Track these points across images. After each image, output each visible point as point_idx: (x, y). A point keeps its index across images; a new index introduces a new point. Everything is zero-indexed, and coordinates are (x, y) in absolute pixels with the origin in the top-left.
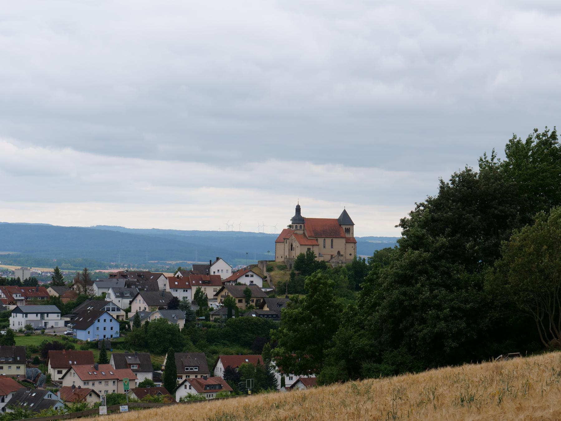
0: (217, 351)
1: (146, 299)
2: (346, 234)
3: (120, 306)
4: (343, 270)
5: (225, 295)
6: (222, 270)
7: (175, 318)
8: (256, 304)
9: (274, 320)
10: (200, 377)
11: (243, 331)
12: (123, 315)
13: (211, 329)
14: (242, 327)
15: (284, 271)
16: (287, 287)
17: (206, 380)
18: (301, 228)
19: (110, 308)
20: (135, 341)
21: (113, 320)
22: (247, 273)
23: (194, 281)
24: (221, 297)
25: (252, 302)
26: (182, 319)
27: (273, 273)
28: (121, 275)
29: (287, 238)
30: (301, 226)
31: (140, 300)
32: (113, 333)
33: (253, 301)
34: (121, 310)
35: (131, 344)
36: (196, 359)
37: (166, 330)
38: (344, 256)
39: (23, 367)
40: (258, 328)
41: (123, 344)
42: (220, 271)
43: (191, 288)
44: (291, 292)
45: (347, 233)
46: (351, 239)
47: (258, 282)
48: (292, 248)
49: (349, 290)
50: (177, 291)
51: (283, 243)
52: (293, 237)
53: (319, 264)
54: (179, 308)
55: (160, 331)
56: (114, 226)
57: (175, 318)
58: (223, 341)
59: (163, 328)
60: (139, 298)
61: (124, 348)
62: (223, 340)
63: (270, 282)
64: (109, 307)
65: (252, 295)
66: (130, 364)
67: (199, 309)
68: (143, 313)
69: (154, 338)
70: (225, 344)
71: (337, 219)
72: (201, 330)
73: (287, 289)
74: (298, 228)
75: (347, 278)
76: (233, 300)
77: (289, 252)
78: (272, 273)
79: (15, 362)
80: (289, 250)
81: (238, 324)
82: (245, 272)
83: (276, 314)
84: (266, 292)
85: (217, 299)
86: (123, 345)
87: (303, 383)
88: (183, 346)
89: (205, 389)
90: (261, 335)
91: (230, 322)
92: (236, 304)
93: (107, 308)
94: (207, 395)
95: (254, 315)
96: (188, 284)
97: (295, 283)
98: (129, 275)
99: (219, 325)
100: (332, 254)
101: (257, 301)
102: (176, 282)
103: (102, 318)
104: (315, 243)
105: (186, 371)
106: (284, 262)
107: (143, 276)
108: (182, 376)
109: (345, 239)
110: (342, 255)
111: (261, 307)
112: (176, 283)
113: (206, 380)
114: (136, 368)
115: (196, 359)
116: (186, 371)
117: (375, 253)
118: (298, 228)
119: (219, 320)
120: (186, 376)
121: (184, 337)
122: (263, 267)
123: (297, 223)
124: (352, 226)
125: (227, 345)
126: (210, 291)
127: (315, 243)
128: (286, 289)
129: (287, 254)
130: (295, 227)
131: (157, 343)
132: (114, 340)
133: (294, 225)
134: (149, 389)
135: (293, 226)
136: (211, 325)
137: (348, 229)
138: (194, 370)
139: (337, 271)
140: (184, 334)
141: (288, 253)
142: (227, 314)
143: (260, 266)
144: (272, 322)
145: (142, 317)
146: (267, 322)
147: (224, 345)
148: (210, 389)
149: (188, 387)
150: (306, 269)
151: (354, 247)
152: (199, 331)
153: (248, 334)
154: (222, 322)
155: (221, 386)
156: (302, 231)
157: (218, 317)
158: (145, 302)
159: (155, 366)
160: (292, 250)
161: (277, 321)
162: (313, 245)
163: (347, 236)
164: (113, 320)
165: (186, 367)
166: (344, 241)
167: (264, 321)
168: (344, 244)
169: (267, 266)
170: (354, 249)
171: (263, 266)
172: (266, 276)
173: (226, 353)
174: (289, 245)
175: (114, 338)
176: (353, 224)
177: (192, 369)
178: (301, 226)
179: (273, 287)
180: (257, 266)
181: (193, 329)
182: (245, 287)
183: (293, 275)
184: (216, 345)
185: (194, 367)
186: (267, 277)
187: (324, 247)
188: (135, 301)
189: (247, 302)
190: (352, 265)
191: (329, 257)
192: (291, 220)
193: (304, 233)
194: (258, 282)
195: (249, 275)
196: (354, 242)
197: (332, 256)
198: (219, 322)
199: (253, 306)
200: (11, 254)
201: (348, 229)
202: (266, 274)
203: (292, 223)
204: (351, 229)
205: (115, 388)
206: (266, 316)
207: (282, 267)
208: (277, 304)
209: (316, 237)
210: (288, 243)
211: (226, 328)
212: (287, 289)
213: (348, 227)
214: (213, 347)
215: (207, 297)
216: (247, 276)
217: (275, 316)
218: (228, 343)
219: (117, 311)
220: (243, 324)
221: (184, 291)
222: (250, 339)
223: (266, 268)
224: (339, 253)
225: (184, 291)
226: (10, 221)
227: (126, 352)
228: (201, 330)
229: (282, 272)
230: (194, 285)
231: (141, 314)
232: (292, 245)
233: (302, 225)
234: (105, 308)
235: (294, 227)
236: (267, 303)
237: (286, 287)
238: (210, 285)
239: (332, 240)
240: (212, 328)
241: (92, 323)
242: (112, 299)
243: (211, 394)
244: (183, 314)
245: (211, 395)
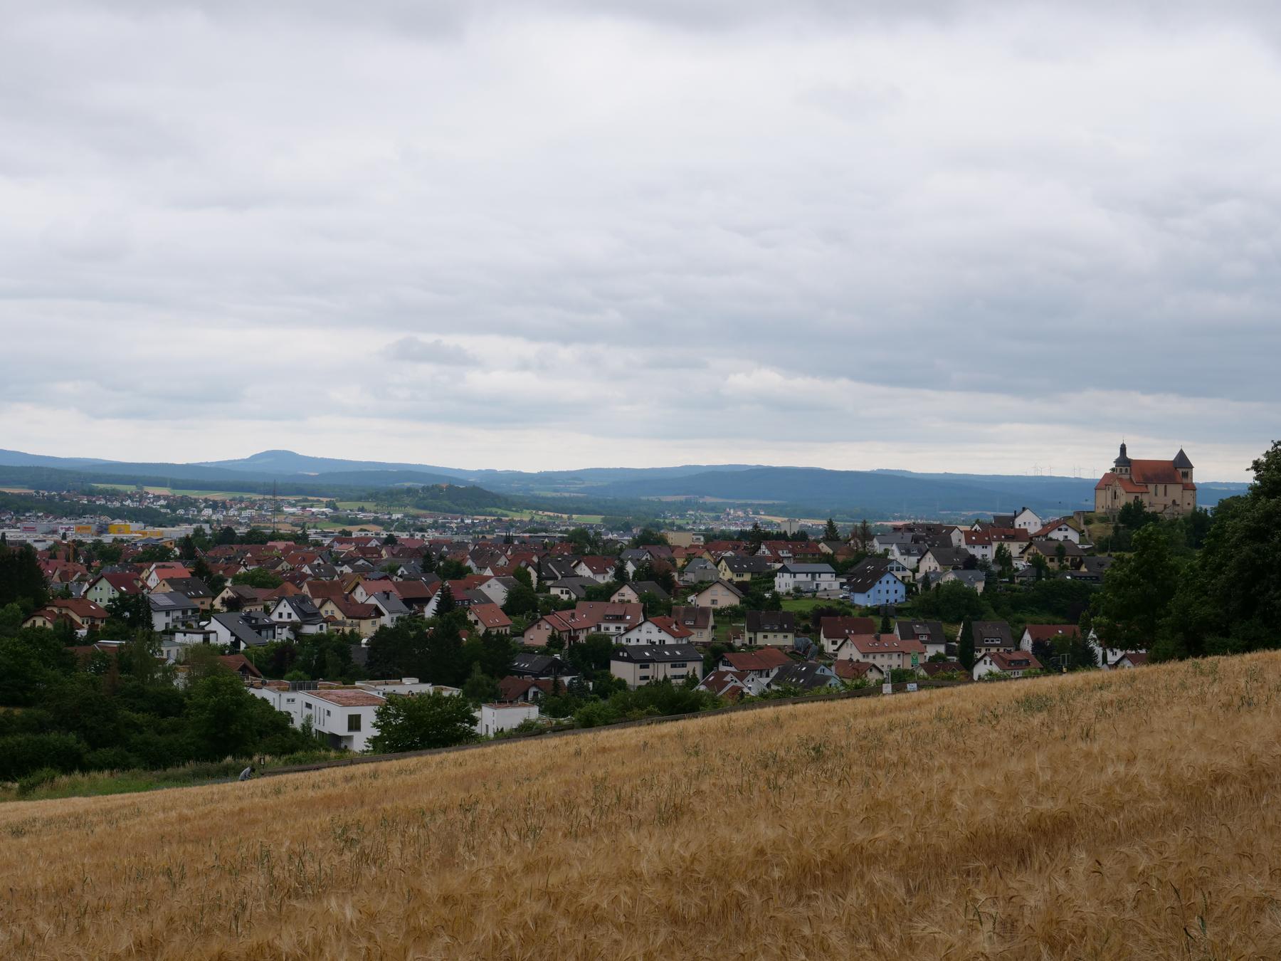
1: (936, 558)
26: (981, 581)
32: (898, 596)
39: (791, 636)
43: (991, 544)
47: (1074, 537)
48: (1115, 496)
52: (1117, 483)
60: (929, 555)
61: (911, 615)
65: (1067, 553)
74: (1124, 472)
75: (1184, 533)
78: (1091, 527)
79: (781, 630)
82: (1057, 525)
95: (1069, 577)
101: (1072, 560)
103: (884, 579)
106: (1105, 513)
110: (1178, 505)
112: (974, 538)
114: (925, 638)
118: (1124, 472)
120: (617, 628)
126: (1014, 548)
129: (1109, 503)
139: (1172, 523)
147: (1032, 612)
149: (988, 663)
163: (1185, 481)
166: (1180, 487)
176: (1192, 467)
177: (993, 641)
183: (1116, 529)
189: (1060, 561)
194: (1074, 537)
197: (1165, 505)
202: (1083, 527)
205: (900, 662)
207: (1103, 520)
213: (1184, 470)
214: (1019, 615)
216: (1060, 530)
224: (1174, 502)
229: (1103, 525)
230: (995, 540)
232: (1115, 493)
233: (1128, 468)
241: (872, 585)
244: (982, 575)
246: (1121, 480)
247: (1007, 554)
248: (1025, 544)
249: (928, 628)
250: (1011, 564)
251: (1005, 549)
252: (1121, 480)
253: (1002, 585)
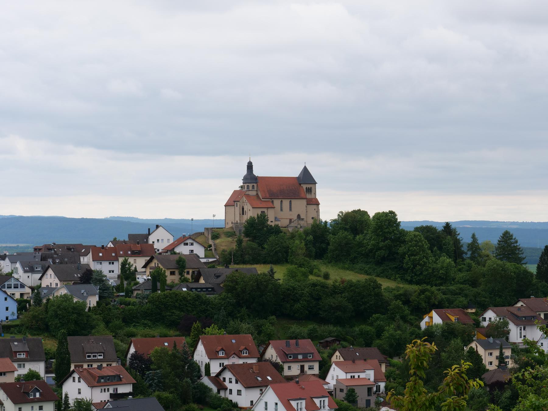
0: (136, 333)
1: (58, 274)
2: (308, 194)
3: (25, 283)
6: (162, 240)
7: (85, 294)
8: (192, 276)
9: (207, 294)
10: (106, 366)
12: (29, 293)
13: (130, 306)
14: (167, 303)
15: (231, 239)
16: (232, 257)
17: (101, 370)
18: (254, 188)
19: (11, 284)
20: (32, 322)
21: (8, 299)
22: (186, 240)
25: (187, 274)
26: (95, 295)
27: (219, 241)
28: (47, 249)
29: (237, 200)
30: (253, 186)
31: (51, 275)
33: (188, 273)
35: (27, 328)
36: (101, 343)
37: (70, 309)
42: (160, 241)
44: (238, 262)
45: (309, 194)
46: (314, 200)
47: (199, 251)
48: (243, 212)
50: (101, 263)
51: (234, 207)
52: (244, 199)
54: (91, 282)
56: (127, 217)
57: (85, 294)
58: (143, 321)
59: (67, 306)
60: (50, 272)
61: (20, 332)
62: (144, 320)
63: (215, 251)
64: (11, 283)
65: (187, 266)
66: (16, 352)
67: (120, 284)
68: (46, 290)
70: (146, 324)
72: (118, 308)
74: (251, 188)
76: (163, 271)
77: (240, 216)
78: (218, 241)
80: (240, 214)
81: (162, 299)
82: (182, 241)
83: (212, 287)
87: (230, 371)
88: (93, 327)
89: (99, 382)
91: (152, 297)
92: (166, 276)
93: (7, 284)
95: (185, 289)
96: (114, 255)
98: (56, 249)
101: (193, 272)
102: (101, 253)
105: (87, 358)
106: (232, 228)
107: (74, 249)
108: (83, 365)
109: (306, 200)
110: (303, 219)
111: (196, 279)
112: (101, 254)
113: (101, 370)
114: (23, 356)
115: (101, 343)
116: (87, 358)
117: (339, 215)
118: (251, 188)
119: (139, 296)
120: (88, 366)
121: (94, 317)
123: (249, 183)
124: (314, 185)
125: (149, 326)
127: (271, 205)
128: (231, 259)
129: (238, 219)
130: (246, 187)
131: (59, 325)
132: (9, 323)
133: (246, 185)
135: (244, 186)
136: (130, 302)
137: (310, 188)
138: (98, 358)
139: (293, 236)
142: (151, 288)
146: (198, 297)
147: (145, 325)
148: (105, 382)
149: (77, 380)
150: (257, 234)
151: (316, 209)
152: (114, 310)
154: (144, 298)
155: (120, 377)
156: (255, 192)
157: (139, 292)
159: (51, 354)
160: (243, 214)
163: (309, 196)
164: (8, 299)
165: (87, 354)
166: (304, 202)
168: (305, 206)
170: (317, 212)
171: (209, 233)
172: (211, 245)
176: (315, 183)
177: (95, 356)
178: (253, 186)
180: (204, 234)
181: (106, 307)
182: (179, 256)
183: (240, 242)
184: (135, 326)
185: (97, 353)
186: (212, 245)
187: (281, 210)
189: (181, 274)
193: (257, 194)
194: (199, 251)
195: (188, 243)
196: (317, 204)
197: (291, 220)
198: (139, 298)
201: (310, 188)
202: (211, 242)
203: (243, 183)
206: (199, 290)
207: (230, 234)
208: (215, 275)
209: (271, 199)
210: (238, 206)
211: (148, 306)
213: (309, 186)
214: (132, 329)
216: (187, 244)
217: (211, 290)
218: (149, 323)
219: (20, 288)
220: (168, 300)
221: (110, 263)
222: (177, 317)
223: (211, 235)
224: (299, 216)
225: (109, 264)
227: (11, 337)
229: (230, 239)
232: (243, 209)
233: (255, 185)
234: (5, 284)
235: (246, 187)
236: (202, 274)
237: (231, 257)
239: (290, 201)
240: (132, 305)
243: (106, 388)
244: (96, 289)
246: (248, 196)
247: (133, 268)
248: (148, 258)
249: (27, 346)
250: (135, 279)
251: (129, 264)
252: (248, 196)
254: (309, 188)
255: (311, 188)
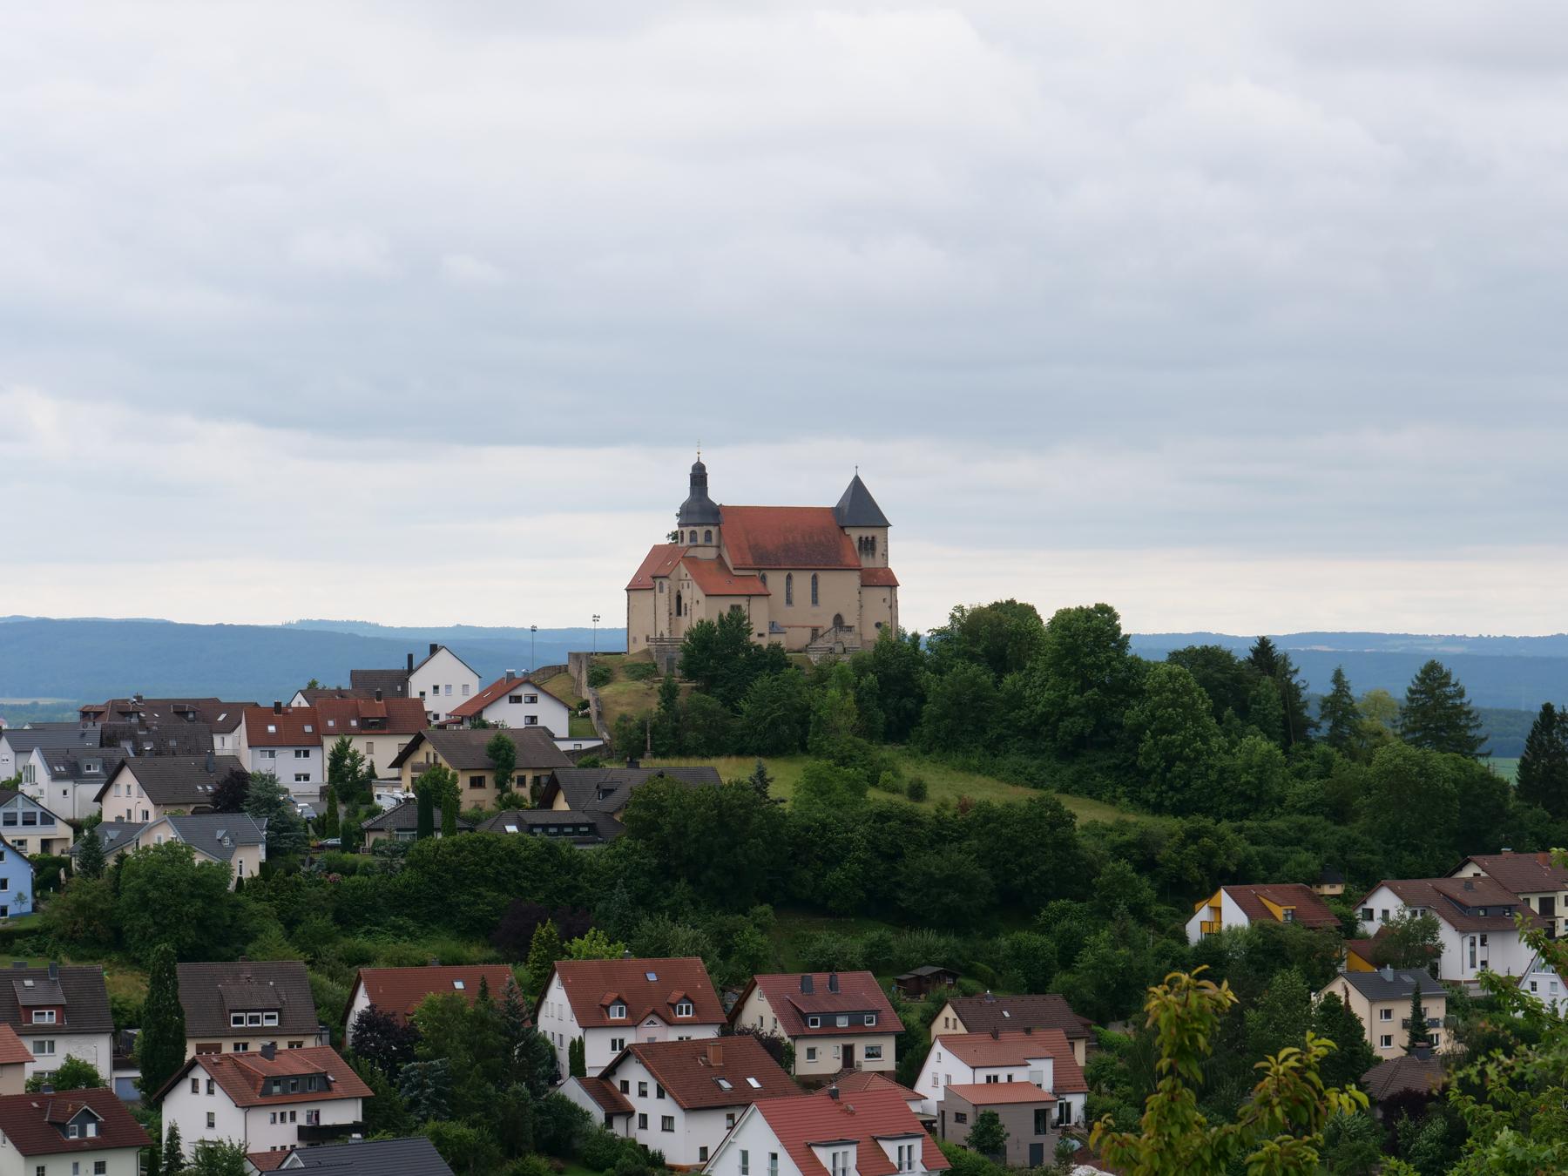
3: (55, 809)
4: (839, 672)
5: (427, 762)
6: (448, 687)
11: (468, 882)
12: (66, 839)
14: (464, 869)
15: (646, 684)
17: (272, 1059)
22: (516, 687)
23: (331, 719)
24: (413, 770)
26: (253, 844)
27: (610, 689)
30: (708, 533)
31: (129, 787)
33: (521, 781)
34: (57, 821)
35: (61, 938)
38: (857, 629)
40: (520, 872)
41: (37, 936)
42: (442, 689)
43: (321, 745)
44: (663, 749)
45: (867, 555)
47: (554, 718)
48: (679, 607)
49: (861, 741)
50: (272, 754)
51: (652, 593)
52: (683, 570)
53: (764, 655)
54: (245, 808)
55: (164, 889)
58: (393, 918)
60: (127, 778)
61: (39, 950)
62: (396, 916)
63: (598, 719)
64: (14, 810)
65: (519, 762)
66: (28, 1008)
69: (142, 914)
70: (400, 928)
71: (832, 508)
72: (319, 883)
73: (649, 741)
75: (851, 698)
76: (449, 777)
77: (670, 619)
78: (606, 691)
80: (671, 614)
82: (506, 689)
83: (591, 822)
84: (578, 751)
85: (399, 779)
86: (34, 940)
87: (642, 1062)
88: (249, 937)
89: (266, 1092)
90: (529, 896)
91: (420, 852)
92: (458, 792)
94: (274, 1114)
95: (512, 829)
97: (677, 721)
99: (384, 864)
100: (816, 623)
101: (537, 780)
102: (271, 724)
104: (756, 587)
105: (233, 1026)
106: (647, 652)
107: (194, 712)
108: (221, 1044)
109: (858, 573)
110: (850, 628)
112: (272, 729)
113: (272, 1059)
114: (49, 1019)
115: (271, 983)
116: (233, 1026)
117: (953, 616)
118: (701, 540)
120: (236, 1047)
122: (580, 672)
123: (695, 525)
125: (411, 935)
126: (379, 753)
127: (756, 587)
128: (645, 742)
129: (663, 628)
132: (10, 924)
133: (687, 531)
134: (49, 1096)
135: (682, 532)
137: (870, 539)
138: (265, 1025)
139: (821, 678)
140: (256, 898)
141: (668, 623)
143: (573, 670)
144: (570, 850)
145: (112, 840)
146: (551, 850)
147: (399, 932)
148: (284, 1092)
152: (310, 887)
153: (484, 894)
154: (395, 853)
155: (326, 1078)
157: (382, 836)
158: (145, 794)
159: (130, 1012)
160: (679, 613)
161: (591, 847)
162: (749, 596)
163: (867, 562)
165: (233, 1015)
166: (854, 579)
167: (543, 846)
169: (590, 666)
170: (890, 607)
171: (581, 667)
173: (400, 959)
174: (669, 597)
175: (10, 916)
176: (885, 525)
177: (254, 1020)
178: (708, 533)
179: (605, 734)
180: (566, 671)
183: (669, 693)
184: (368, 932)
185: (262, 1011)
187: (789, 602)
188: (112, 791)
189: (501, 784)
190: (875, 655)
191: (808, 634)
192: (677, 515)
193: (720, 557)
194: (554, 718)
195: (520, 697)
196: (892, 584)
197: (815, 630)
198: (382, 853)
199: (522, 797)
200: (41, 703)
201: (870, 539)
202: (587, 693)
203: (680, 525)
204: (879, 540)
206: (552, 830)
207: (642, 670)
208: (598, 787)
209: (759, 569)
210: (666, 590)
211: (407, 874)
212: (649, 741)
214: (361, 942)
215: (372, 773)
216: (517, 699)
217: (586, 829)
218: (411, 925)
219: (42, 823)
221: (298, 754)
224: (838, 620)
226: (55, 615)
228: (319, 883)
229: (641, 685)
230: (330, 734)
231: (109, 832)
232: (679, 598)
233: (714, 530)
235: (687, 536)
236: (562, 786)
237: (646, 735)
238: (386, 732)
239: (815, 578)
240: (361, 874)
242: (39, 787)
243: (288, 1110)
244: (259, 827)
245: (288, 1116)
246: (693, 562)
247: (363, 768)
248: (407, 740)
251: (353, 756)
252: (693, 562)
253: (317, 857)
254: (867, 538)
255: (873, 538)
